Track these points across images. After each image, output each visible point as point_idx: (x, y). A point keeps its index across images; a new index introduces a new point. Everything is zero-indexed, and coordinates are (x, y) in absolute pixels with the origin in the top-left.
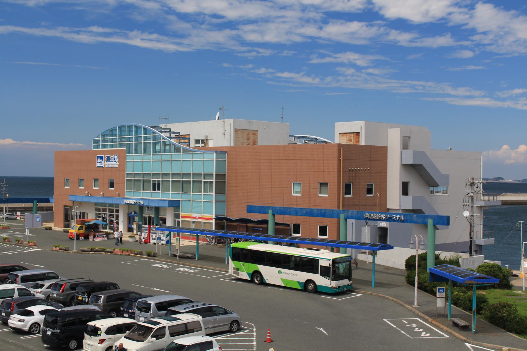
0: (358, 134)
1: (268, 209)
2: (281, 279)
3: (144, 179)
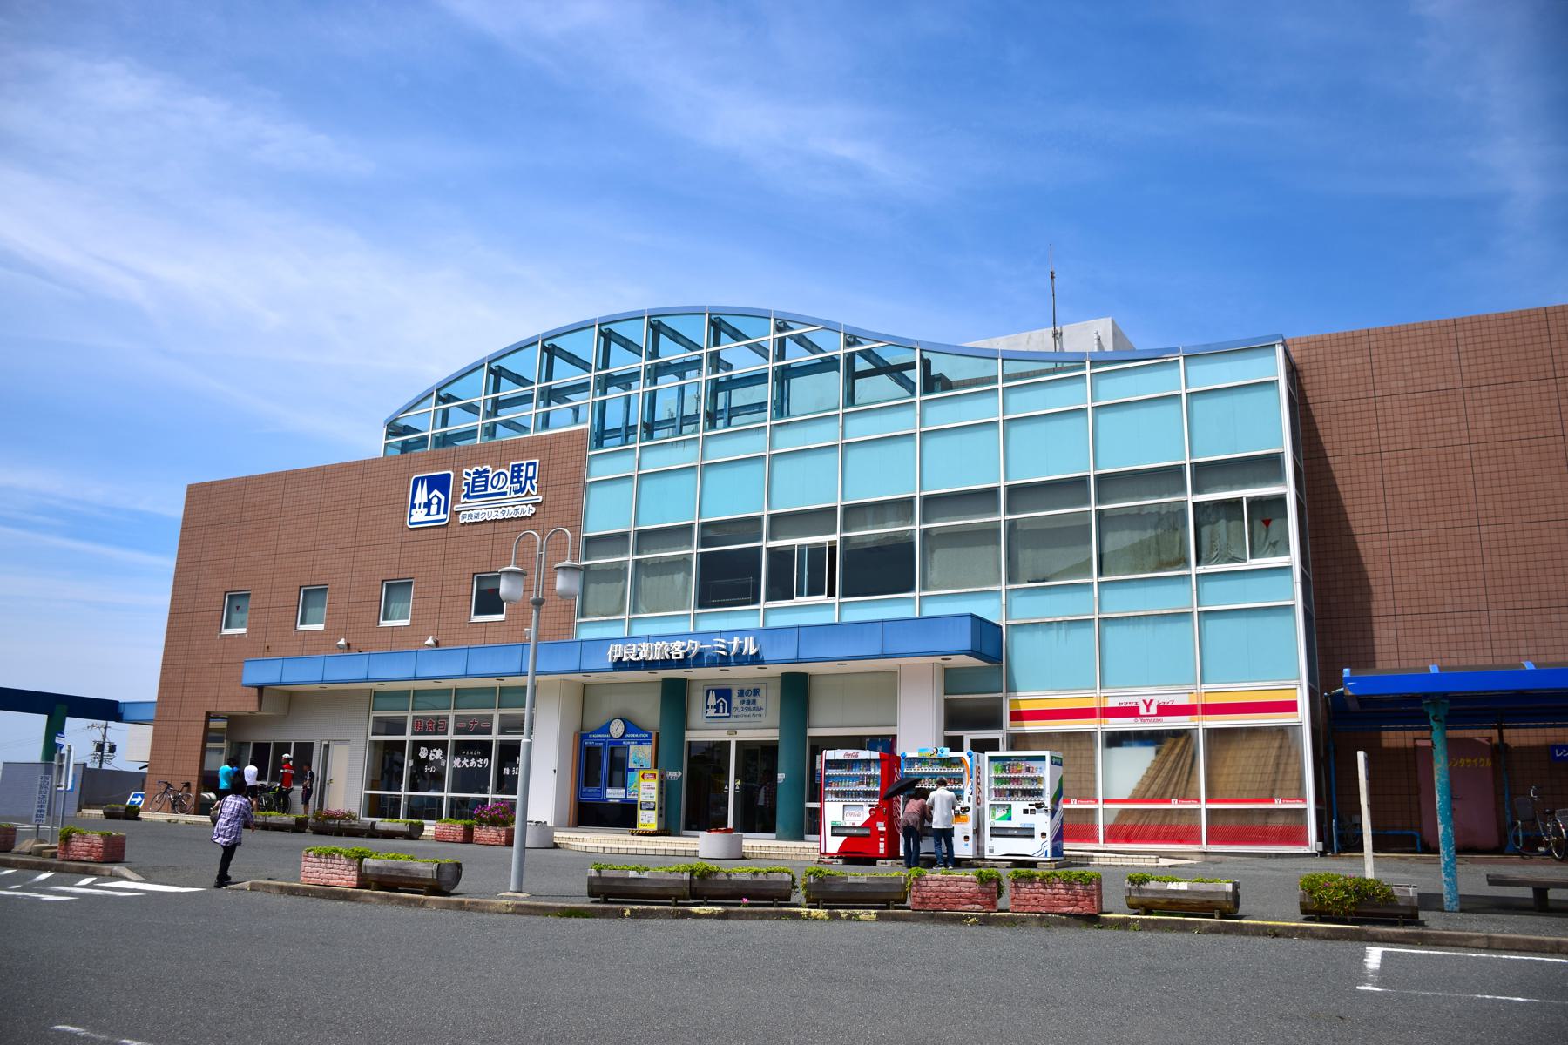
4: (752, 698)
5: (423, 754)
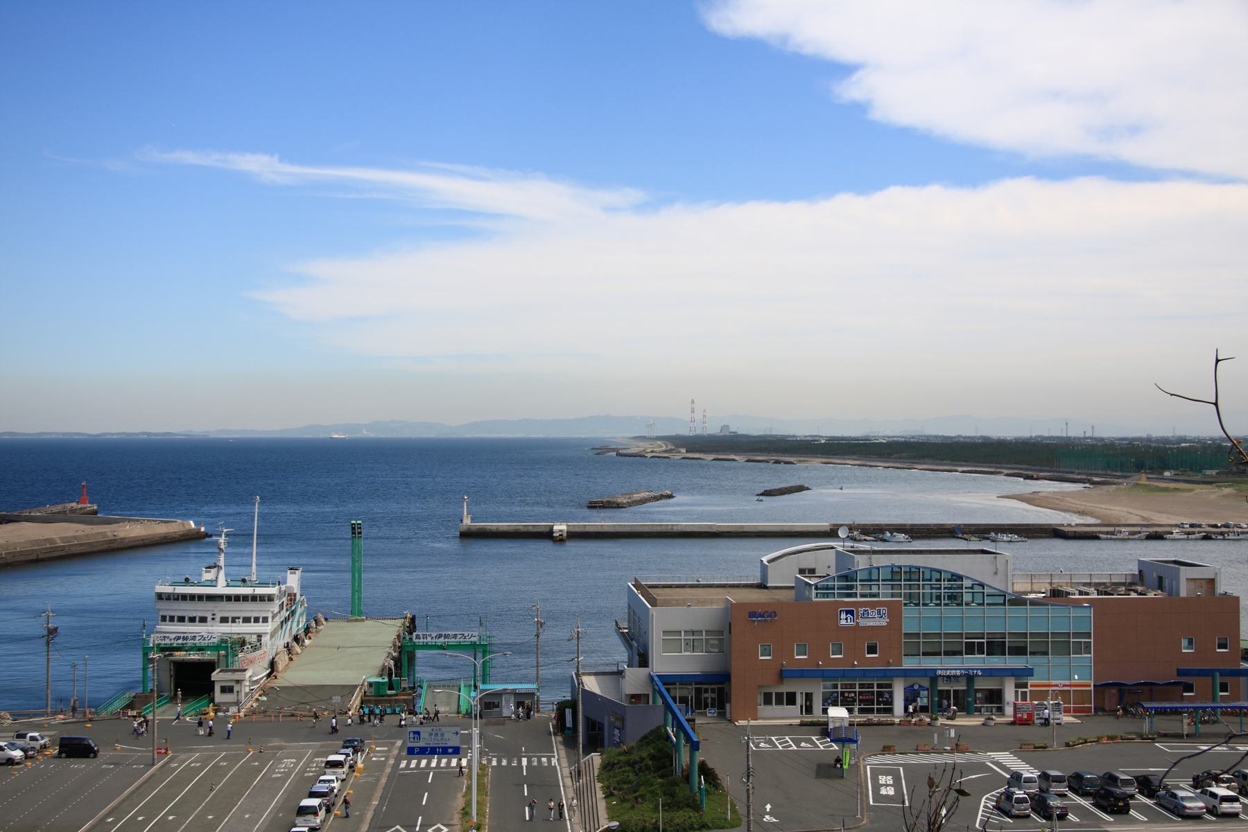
5: (846, 695)
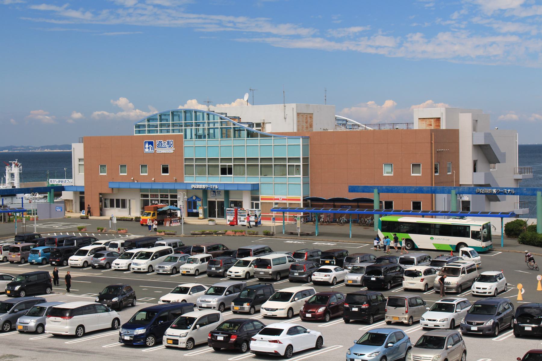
0: (438, 119)
1: (373, 188)
2: (433, 244)
3: (196, 164)
4: (219, 193)
